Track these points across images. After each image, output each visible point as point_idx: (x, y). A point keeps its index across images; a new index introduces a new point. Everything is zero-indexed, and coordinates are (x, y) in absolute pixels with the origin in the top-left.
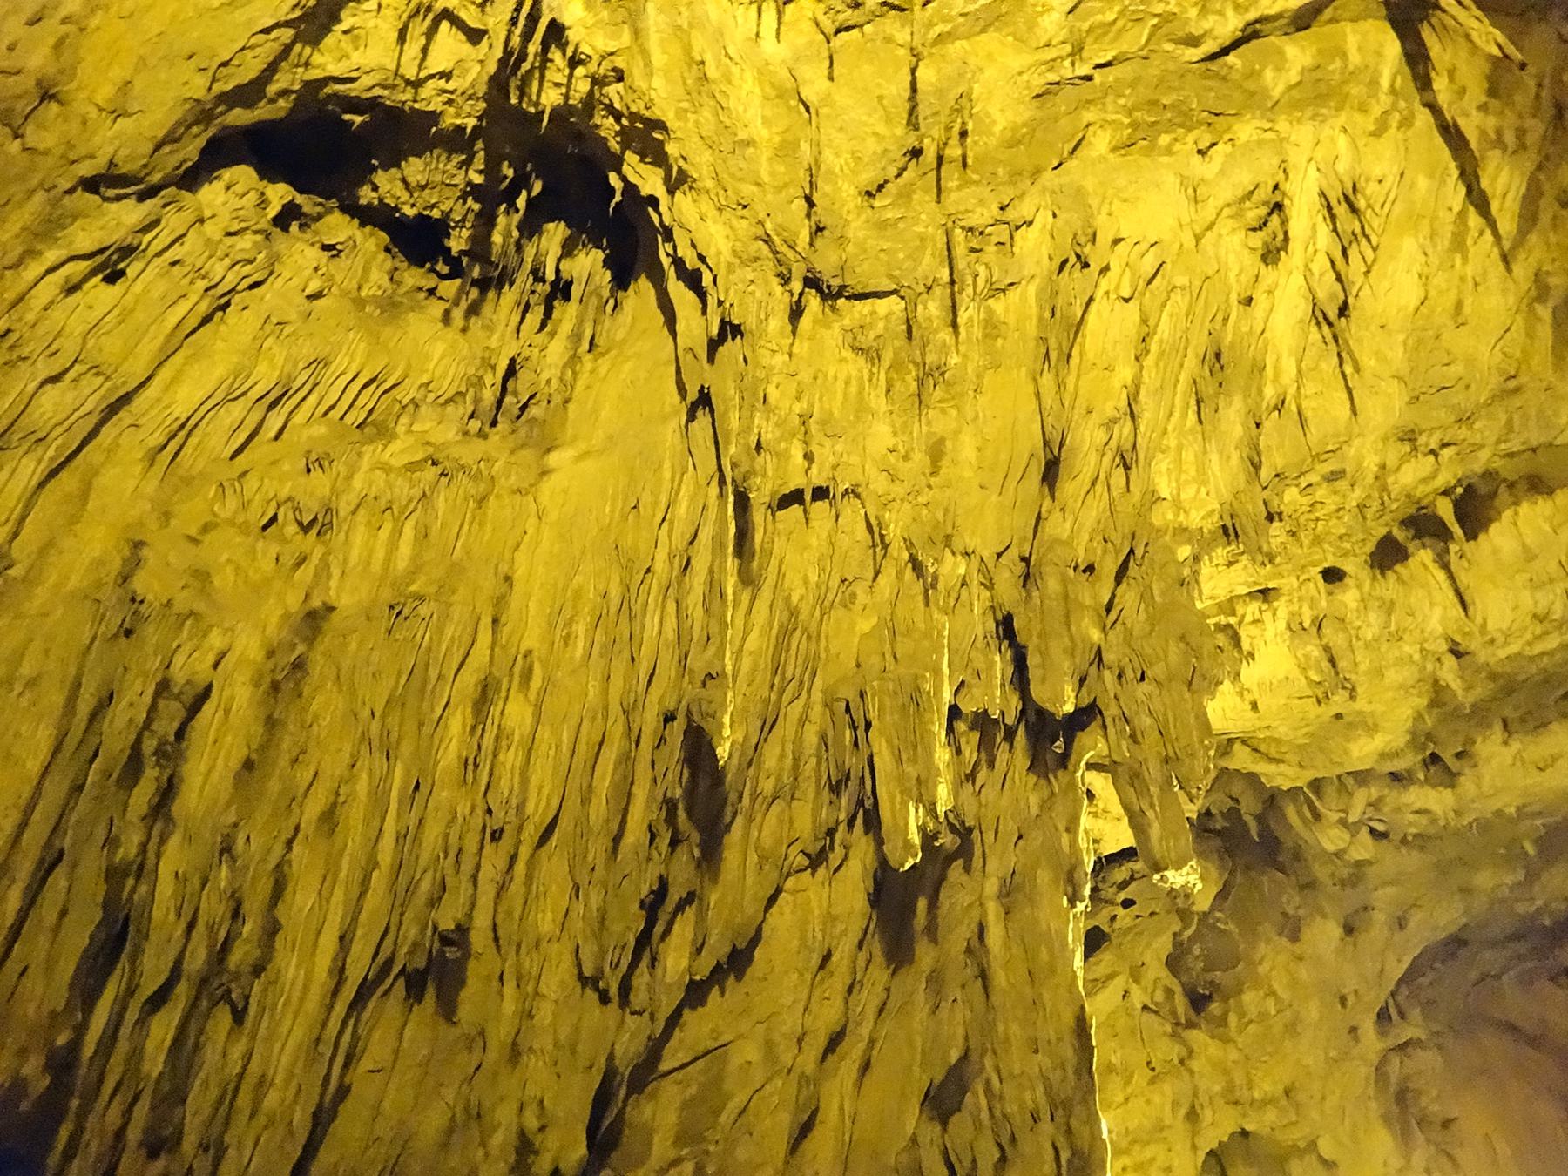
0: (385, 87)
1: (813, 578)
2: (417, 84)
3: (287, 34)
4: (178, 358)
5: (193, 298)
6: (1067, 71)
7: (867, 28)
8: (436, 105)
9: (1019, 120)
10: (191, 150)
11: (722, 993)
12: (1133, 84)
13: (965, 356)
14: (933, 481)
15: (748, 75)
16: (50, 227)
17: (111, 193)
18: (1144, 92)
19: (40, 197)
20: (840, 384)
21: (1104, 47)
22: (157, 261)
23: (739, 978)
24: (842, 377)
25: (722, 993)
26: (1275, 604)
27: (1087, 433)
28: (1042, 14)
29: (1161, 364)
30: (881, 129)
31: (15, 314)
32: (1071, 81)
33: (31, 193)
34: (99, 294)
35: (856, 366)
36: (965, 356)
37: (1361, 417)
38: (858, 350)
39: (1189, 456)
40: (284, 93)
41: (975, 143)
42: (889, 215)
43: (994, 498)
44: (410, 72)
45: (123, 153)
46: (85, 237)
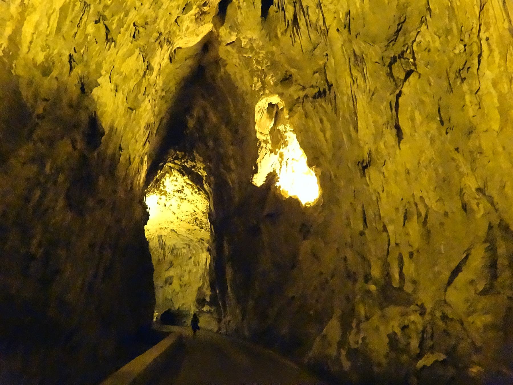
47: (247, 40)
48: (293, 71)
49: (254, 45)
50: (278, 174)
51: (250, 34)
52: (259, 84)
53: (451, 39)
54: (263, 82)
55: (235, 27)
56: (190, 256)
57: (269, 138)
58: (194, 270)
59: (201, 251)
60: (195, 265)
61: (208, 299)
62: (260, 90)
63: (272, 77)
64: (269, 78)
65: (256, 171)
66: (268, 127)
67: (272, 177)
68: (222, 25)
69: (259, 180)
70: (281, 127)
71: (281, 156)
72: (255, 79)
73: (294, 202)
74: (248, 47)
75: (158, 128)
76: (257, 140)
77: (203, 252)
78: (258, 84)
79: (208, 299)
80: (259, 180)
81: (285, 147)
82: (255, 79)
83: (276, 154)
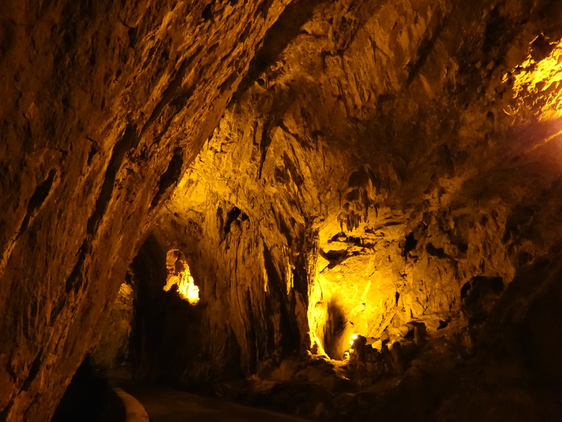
10: (224, 232)
16: (221, 249)
34: (228, 251)
46: (224, 248)
51: (165, 226)
52: (170, 244)
53: (477, 62)
56: (111, 321)
57: (174, 267)
58: (115, 333)
59: (121, 318)
60: (116, 329)
61: (126, 357)
62: (170, 246)
65: (165, 284)
67: (175, 287)
69: (167, 288)
71: (181, 275)
73: (186, 302)
76: (167, 269)
77: (123, 319)
79: (126, 357)
80: (167, 288)
83: (177, 276)
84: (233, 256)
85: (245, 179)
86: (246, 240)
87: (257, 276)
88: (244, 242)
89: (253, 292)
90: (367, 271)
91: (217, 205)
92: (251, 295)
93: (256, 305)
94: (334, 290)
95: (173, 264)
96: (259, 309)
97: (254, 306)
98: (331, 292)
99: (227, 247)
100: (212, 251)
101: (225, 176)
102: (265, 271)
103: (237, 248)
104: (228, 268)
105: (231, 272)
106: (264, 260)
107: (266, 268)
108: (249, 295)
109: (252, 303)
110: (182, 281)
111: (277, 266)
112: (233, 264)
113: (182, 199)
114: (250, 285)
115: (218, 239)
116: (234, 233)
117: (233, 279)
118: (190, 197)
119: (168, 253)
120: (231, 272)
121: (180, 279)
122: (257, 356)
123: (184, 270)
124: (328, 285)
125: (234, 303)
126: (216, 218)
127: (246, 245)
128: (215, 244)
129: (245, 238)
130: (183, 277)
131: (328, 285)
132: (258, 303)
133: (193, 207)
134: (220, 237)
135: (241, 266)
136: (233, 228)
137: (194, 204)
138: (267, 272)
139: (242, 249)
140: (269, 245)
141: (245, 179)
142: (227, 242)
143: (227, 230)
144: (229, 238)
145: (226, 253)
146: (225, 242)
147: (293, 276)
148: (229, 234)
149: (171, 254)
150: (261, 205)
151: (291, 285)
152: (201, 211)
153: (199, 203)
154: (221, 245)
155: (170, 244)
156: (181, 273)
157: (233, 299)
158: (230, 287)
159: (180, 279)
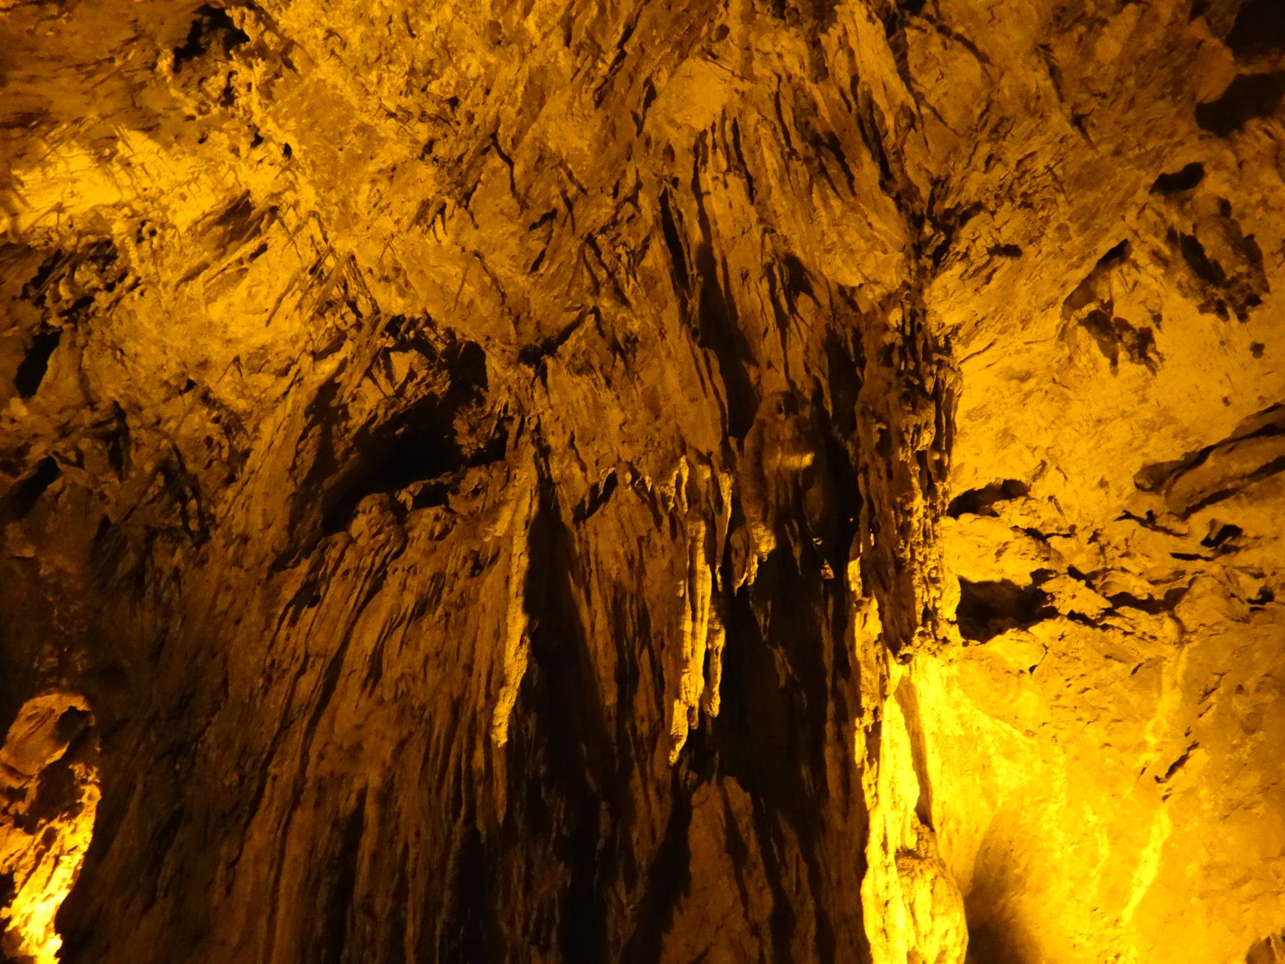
0: (392, 407)
1: (621, 551)
2: (400, 392)
3: (317, 429)
4: (360, 621)
5: (360, 584)
6: (603, 69)
7: (482, 177)
8: (423, 392)
9: (596, 130)
10: (315, 515)
11: (681, 911)
12: (654, 24)
13: (642, 316)
14: (658, 424)
15: (448, 266)
16: (271, 598)
17: (290, 563)
18: (665, 21)
19: (258, 590)
20: (582, 403)
21: (614, 28)
22: (333, 580)
23: (687, 894)
24: (581, 397)
25: (681, 911)
26: (1132, 256)
27: (754, 294)
28: (556, 60)
29: (788, 188)
30: (513, 228)
31: (273, 651)
32: (613, 69)
33: (254, 590)
34: (308, 614)
35: (584, 382)
36: (642, 316)
37: (997, 59)
38: (579, 372)
39: (852, 237)
40: (348, 451)
41: (581, 172)
42: (552, 270)
43: (705, 401)
44: (390, 391)
45: (276, 543)
46: (288, 594)
47: (52, 569)
48: (126, 664)
49: (65, 585)
50: (18, 885)
51: (60, 561)
52: (52, 660)
54: (62, 658)
55: (35, 535)
57: (32, 786)
62: (50, 673)
63: (84, 656)
64: (77, 656)
66: (43, 760)
68: (18, 519)
70: (78, 769)
71: (50, 838)
72: (47, 648)
74: (51, 581)
75: (1071, 295)
78: (51, 660)
81: (67, 818)
82: (47, 648)
84: (324, 641)
85: (537, 94)
86: (413, 583)
87: (443, 705)
88: (403, 587)
89: (382, 821)
90: (1152, 741)
91: (329, 366)
92: (368, 843)
93: (382, 904)
94: (1009, 776)
95: (34, 770)
96: (398, 930)
97: (369, 910)
98: (988, 794)
99: (309, 595)
100: (223, 602)
101: (434, 87)
102: (517, 622)
103: (360, 609)
104: (277, 699)
105: (286, 723)
106: (524, 561)
107: (527, 608)
108: (351, 846)
109: (359, 891)
110: (44, 870)
111: (595, 619)
112: (307, 684)
113: (167, 296)
114: (375, 780)
115: (271, 538)
116: (362, 542)
117: (284, 770)
118: (210, 300)
119: (27, 709)
120: (286, 723)
121: (39, 857)
122: (438, 933)
123: (73, 811)
124: (969, 739)
125: (241, 916)
126: (301, 423)
127: (409, 601)
128: (250, 561)
129: (412, 570)
130: (54, 850)
131: (969, 739)
132: (400, 894)
133: (204, 365)
134: (291, 528)
135: (350, 703)
136: (365, 521)
137: (216, 351)
138: (529, 631)
139: (383, 615)
140: (575, 481)
141: (537, 94)
142: (314, 569)
143: (338, 518)
144: (335, 553)
145: (293, 622)
146: (304, 567)
147: (720, 641)
148: (339, 537)
149: (41, 718)
150: (590, 240)
151: (706, 697)
152: (241, 405)
153: (242, 350)
154: (278, 576)
155: (52, 660)
156: (55, 824)
157: (245, 886)
158: (252, 814)
159: (39, 857)
